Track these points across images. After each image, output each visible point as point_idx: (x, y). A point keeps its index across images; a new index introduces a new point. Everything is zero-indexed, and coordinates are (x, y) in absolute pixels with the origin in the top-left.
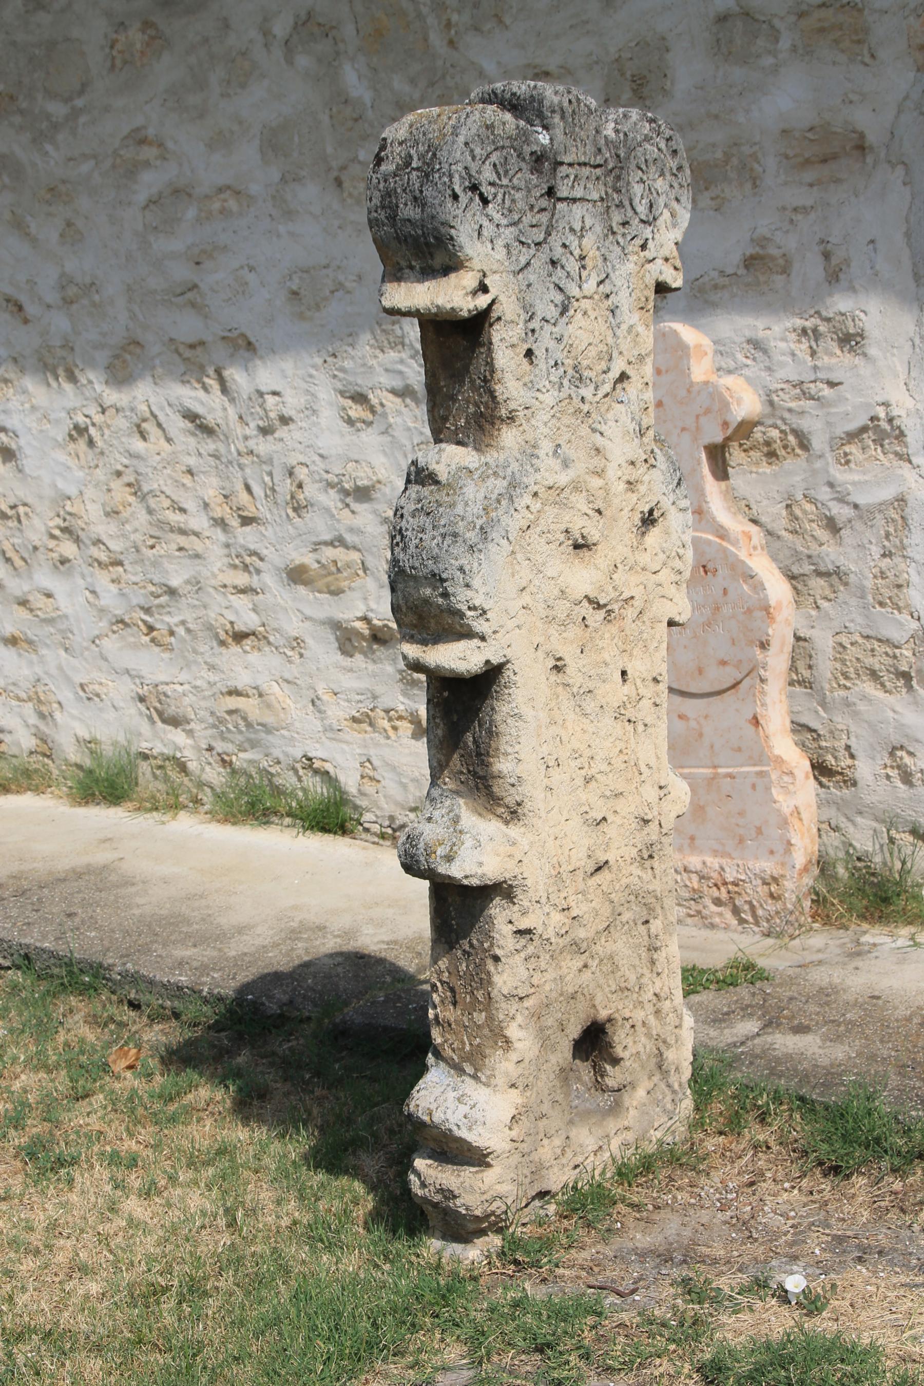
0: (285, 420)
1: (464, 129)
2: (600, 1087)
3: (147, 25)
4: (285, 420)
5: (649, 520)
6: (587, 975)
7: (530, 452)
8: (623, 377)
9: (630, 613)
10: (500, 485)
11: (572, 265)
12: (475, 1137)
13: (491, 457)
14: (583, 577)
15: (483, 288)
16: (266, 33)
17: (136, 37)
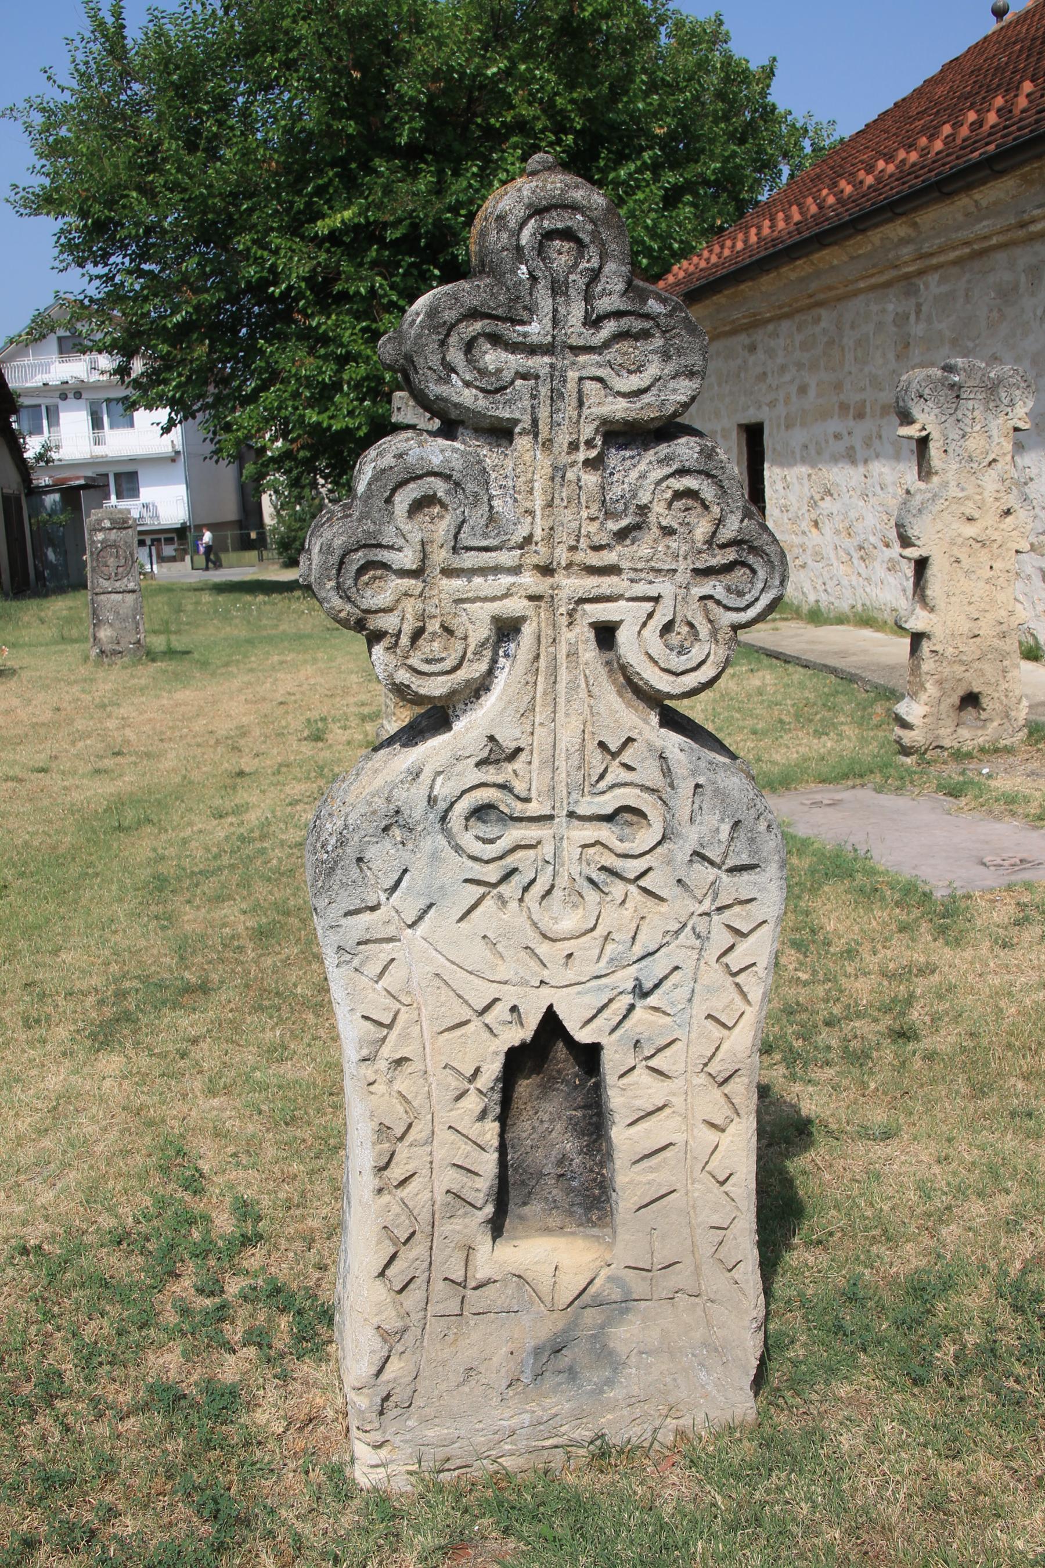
0: (1031, 479)
1: (916, 377)
2: (978, 719)
3: (1000, 310)
4: (1031, 479)
5: (1008, 512)
6: (967, 674)
7: (945, 485)
8: (994, 460)
9: (995, 546)
10: (930, 495)
11: (968, 421)
12: (909, 719)
13: (930, 486)
14: (970, 530)
15: (924, 429)
16: (1035, 315)
17: (995, 314)
